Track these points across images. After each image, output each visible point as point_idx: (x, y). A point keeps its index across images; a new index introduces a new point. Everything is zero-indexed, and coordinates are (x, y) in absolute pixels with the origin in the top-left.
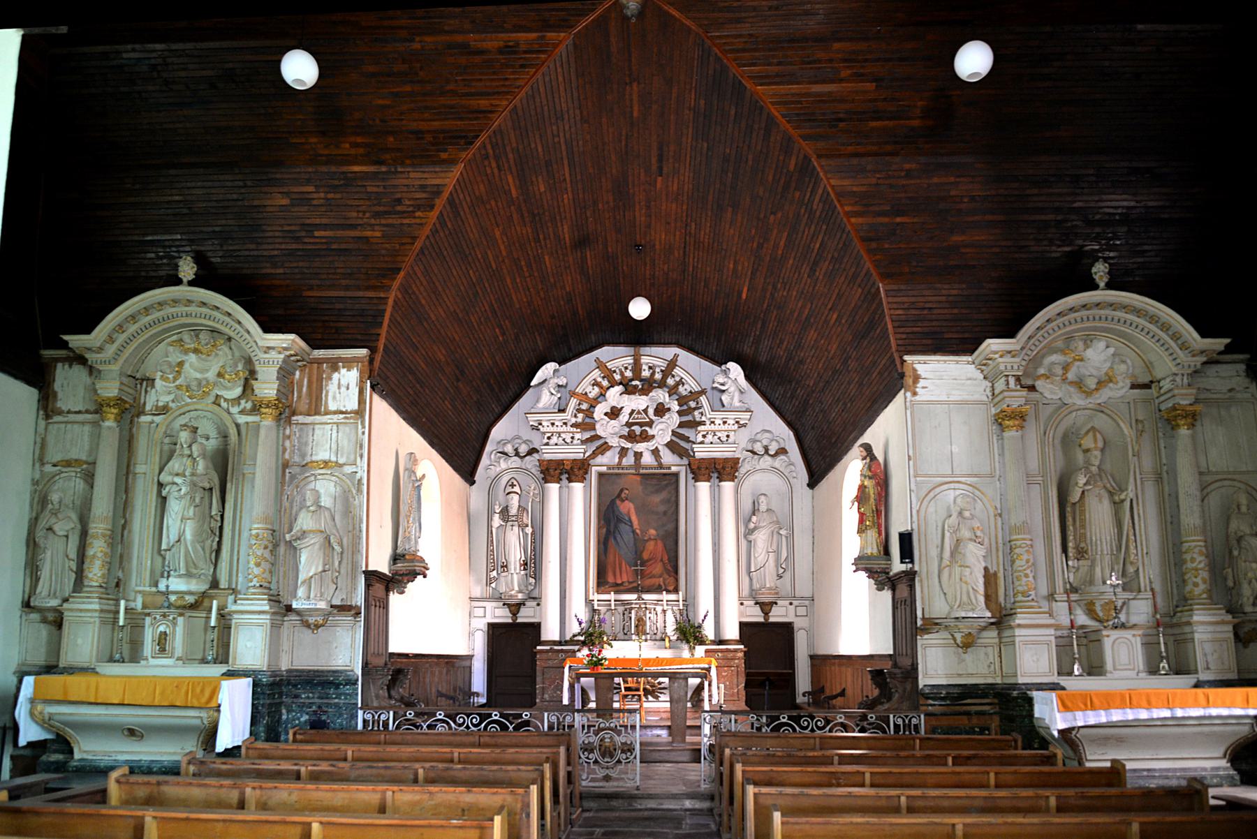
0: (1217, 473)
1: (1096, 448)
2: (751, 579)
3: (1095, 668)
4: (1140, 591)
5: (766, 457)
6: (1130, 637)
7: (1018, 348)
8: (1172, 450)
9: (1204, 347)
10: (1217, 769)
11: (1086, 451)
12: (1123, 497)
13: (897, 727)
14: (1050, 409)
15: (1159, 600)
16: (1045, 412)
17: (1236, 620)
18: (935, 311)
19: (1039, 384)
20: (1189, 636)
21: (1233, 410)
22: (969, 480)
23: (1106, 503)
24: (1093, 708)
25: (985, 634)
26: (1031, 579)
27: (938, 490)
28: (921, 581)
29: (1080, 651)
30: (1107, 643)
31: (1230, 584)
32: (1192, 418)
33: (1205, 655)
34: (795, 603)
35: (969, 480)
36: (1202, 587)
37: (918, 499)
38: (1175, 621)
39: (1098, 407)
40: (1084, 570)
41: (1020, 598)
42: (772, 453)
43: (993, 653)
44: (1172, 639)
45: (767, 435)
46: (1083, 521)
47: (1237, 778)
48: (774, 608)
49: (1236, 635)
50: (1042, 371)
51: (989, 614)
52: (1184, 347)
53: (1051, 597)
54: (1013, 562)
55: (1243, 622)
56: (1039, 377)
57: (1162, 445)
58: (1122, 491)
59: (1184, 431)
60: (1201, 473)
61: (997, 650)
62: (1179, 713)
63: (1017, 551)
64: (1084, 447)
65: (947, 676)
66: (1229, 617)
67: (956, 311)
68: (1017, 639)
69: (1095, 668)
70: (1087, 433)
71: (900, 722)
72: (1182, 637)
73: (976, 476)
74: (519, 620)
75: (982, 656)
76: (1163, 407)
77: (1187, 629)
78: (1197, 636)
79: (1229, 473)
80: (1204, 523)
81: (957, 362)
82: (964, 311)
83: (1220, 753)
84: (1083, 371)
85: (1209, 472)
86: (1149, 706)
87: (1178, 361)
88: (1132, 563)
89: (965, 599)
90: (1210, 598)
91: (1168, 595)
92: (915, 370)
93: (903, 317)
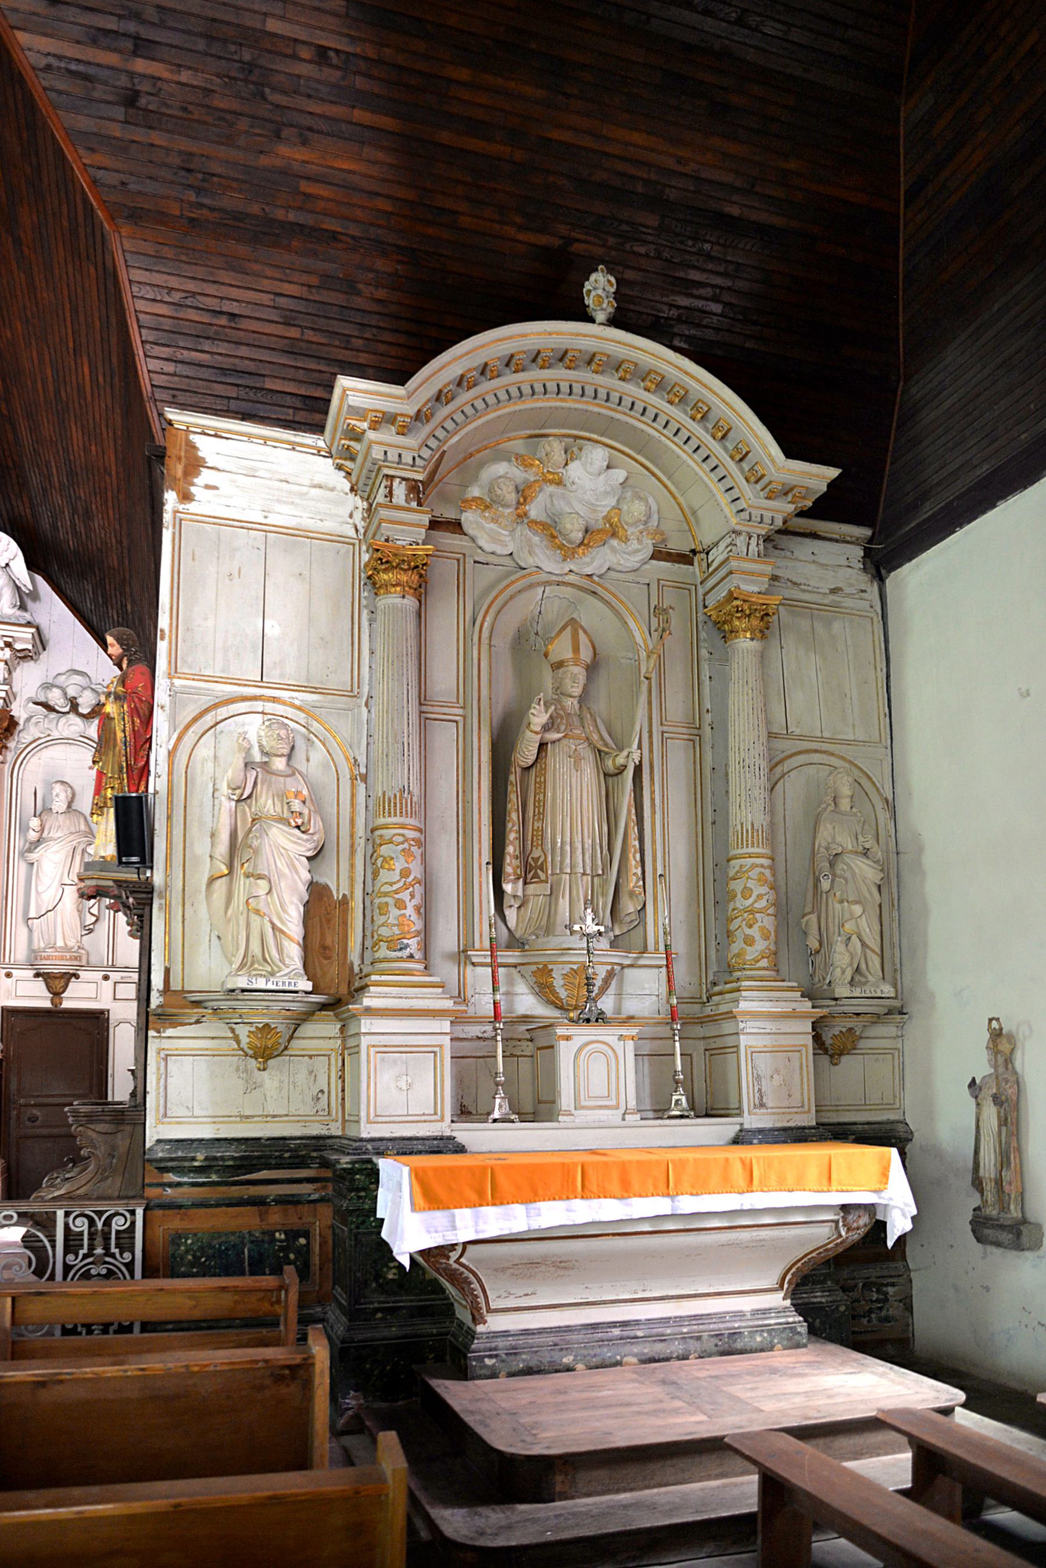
0: (801, 738)
1: (576, 662)
2: (30, 930)
3: (537, 1107)
4: (645, 950)
5: (72, 716)
6: (612, 1040)
7: (412, 411)
8: (722, 682)
9: (791, 479)
10: (765, 1312)
11: (558, 665)
12: (621, 760)
13: (72, 1242)
14: (488, 575)
15: (681, 971)
16: (481, 579)
17: (820, 1012)
18: (244, 324)
19: (469, 518)
20: (730, 1041)
21: (837, 626)
22: (299, 698)
23: (589, 773)
24: (498, 1200)
25: (308, 1029)
26: (410, 911)
27: (223, 712)
28: (167, 908)
29: (504, 1072)
30: (566, 1052)
31: (814, 944)
32: (765, 622)
33: (758, 1078)
34: (115, 976)
35: (299, 698)
36: (760, 945)
37: (173, 726)
38: (708, 1011)
39: (585, 583)
40: (536, 904)
41: (383, 952)
42: (84, 710)
43: (325, 1074)
44: (701, 1045)
45: (78, 679)
46: (540, 804)
47: (803, 1329)
48: (73, 985)
49: (817, 1039)
50: (475, 492)
51: (308, 986)
52: (755, 478)
53: (462, 956)
54: (375, 874)
55: (831, 1016)
56: (467, 503)
57: (706, 673)
58: (621, 749)
59: (745, 644)
60: (771, 735)
61: (336, 1063)
62: (688, 1204)
63: (384, 850)
64: (554, 658)
65: (215, 1119)
66: (807, 1005)
67: (294, 332)
68: (365, 1041)
69: (537, 1107)
70: (564, 628)
71: (81, 1225)
72: (719, 1043)
73: (315, 690)
74: (66, 1004)
75: (302, 1077)
76: (711, 602)
77: (727, 1027)
78: (744, 1041)
79: (822, 740)
80: (772, 824)
81: (293, 446)
82: (310, 335)
83: (771, 1281)
84: (560, 505)
85: (788, 735)
86: (626, 1191)
87: (742, 504)
88: (632, 894)
89: (255, 947)
90: (775, 967)
91: (701, 962)
92: (192, 447)
93: (167, 324)
